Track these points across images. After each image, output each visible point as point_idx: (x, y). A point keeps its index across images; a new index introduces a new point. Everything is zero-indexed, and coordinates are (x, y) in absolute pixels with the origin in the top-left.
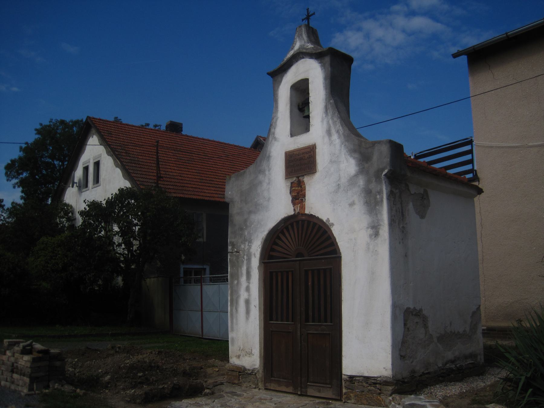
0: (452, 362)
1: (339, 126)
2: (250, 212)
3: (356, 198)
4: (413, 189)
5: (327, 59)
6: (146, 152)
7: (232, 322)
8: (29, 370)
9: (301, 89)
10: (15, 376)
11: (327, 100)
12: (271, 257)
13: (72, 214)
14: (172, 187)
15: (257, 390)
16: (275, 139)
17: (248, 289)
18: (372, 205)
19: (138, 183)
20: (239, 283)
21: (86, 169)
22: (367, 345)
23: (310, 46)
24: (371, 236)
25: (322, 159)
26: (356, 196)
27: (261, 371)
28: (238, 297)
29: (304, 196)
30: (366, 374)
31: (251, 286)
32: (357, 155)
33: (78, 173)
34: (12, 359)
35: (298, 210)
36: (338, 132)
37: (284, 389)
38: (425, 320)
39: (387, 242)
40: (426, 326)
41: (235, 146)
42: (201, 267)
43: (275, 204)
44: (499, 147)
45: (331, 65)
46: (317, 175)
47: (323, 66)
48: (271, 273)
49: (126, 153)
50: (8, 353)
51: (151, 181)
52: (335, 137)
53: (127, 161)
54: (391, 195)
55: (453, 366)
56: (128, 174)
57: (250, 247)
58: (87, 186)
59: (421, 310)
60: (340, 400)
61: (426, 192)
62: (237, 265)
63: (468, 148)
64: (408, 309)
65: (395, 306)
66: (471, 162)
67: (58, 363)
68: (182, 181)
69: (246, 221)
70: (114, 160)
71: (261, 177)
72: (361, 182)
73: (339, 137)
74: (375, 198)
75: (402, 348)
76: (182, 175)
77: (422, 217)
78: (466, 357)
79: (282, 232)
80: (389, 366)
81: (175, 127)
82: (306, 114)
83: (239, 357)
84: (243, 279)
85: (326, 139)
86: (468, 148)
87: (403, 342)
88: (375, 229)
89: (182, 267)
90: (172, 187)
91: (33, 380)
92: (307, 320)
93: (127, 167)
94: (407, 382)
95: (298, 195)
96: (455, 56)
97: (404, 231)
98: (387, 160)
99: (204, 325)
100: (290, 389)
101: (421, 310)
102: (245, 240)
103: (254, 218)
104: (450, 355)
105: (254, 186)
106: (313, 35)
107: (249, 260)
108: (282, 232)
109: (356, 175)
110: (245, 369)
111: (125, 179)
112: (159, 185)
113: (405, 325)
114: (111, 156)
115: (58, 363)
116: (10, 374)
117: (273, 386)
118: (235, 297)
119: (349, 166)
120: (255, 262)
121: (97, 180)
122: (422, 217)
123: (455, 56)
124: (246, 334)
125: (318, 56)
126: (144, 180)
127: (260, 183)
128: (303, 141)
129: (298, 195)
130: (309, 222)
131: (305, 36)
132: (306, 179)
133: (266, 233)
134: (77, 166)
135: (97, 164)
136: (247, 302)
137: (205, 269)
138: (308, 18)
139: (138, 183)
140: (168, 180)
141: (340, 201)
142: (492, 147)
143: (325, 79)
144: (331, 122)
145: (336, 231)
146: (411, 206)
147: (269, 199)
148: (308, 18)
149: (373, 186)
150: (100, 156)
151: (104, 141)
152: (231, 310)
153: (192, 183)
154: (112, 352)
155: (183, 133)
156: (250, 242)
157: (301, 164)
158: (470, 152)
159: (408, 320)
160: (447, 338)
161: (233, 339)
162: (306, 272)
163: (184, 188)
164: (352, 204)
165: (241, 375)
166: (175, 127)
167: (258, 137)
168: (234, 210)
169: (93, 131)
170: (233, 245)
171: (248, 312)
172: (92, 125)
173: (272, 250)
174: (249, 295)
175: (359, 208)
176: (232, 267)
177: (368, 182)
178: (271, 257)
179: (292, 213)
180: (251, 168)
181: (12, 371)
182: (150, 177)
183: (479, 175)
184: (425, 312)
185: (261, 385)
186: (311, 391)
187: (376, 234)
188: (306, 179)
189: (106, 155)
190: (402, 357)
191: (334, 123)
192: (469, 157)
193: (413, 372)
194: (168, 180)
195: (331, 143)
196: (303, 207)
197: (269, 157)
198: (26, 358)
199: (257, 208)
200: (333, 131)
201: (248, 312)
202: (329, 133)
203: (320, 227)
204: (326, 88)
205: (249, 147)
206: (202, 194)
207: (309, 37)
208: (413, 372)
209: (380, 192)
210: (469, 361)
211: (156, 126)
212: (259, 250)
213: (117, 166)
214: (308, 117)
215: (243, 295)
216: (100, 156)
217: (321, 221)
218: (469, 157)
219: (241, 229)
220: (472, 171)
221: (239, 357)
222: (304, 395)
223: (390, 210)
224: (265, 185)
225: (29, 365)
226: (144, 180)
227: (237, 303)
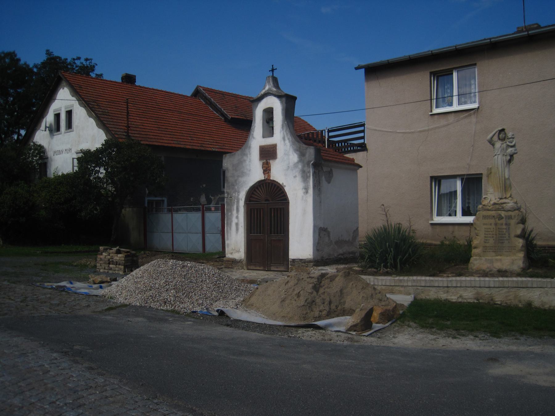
0: (342, 255)
1: (289, 135)
2: (238, 176)
3: (297, 174)
4: (325, 169)
5: (284, 99)
6: (174, 139)
7: (228, 235)
8: (124, 262)
9: (269, 113)
10: (111, 266)
11: (283, 122)
12: (250, 201)
13: (44, 153)
14: (138, 136)
15: (243, 270)
16: (254, 138)
17: (237, 217)
18: (305, 178)
19: (113, 133)
20: (232, 214)
21: (57, 116)
22: (301, 243)
23: (274, 89)
24: (304, 193)
25: (280, 152)
26: (297, 172)
27: (245, 260)
28: (231, 222)
29: (270, 170)
30: (301, 258)
31: (239, 216)
32: (298, 152)
33: (49, 118)
34: (109, 257)
35: (266, 177)
36: (289, 139)
37: (258, 268)
38: (329, 233)
39: (312, 196)
40: (329, 236)
41: (179, 95)
42: (161, 199)
43: (254, 173)
44: (380, 131)
45: (286, 103)
46: (277, 160)
47: (282, 102)
48: (251, 209)
49: (97, 105)
50: (104, 254)
51: (122, 130)
52: (287, 141)
53: (100, 113)
54: (314, 173)
55: (342, 257)
56: (102, 123)
57: (238, 195)
58: (58, 129)
59: (327, 228)
60: (288, 271)
61: (331, 170)
62: (231, 204)
63: (362, 128)
64: (321, 227)
65: (315, 226)
66: (363, 138)
67: (135, 259)
68: (144, 130)
69: (236, 181)
70: (87, 111)
71: (245, 158)
72: (300, 166)
73: (289, 142)
74: (307, 175)
75: (318, 245)
76: (144, 124)
77: (329, 182)
78: (349, 253)
79: (257, 188)
80: (312, 253)
81: (129, 79)
82: (271, 126)
83: (232, 253)
84: (235, 212)
85: (283, 142)
86: (362, 128)
87: (318, 243)
88: (306, 190)
89: (147, 199)
90: (138, 136)
91: (126, 267)
92: (271, 233)
93: (102, 119)
94: (318, 261)
95: (267, 169)
96: (357, 69)
97: (320, 190)
98: (313, 157)
99: (174, 243)
100: (261, 268)
101: (327, 228)
102: (235, 191)
103: (242, 179)
104: (341, 251)
105: (241, 162)
106: (275, 81)
107: (238, 202)
108: (257, 188)
109: (298, 163)
110: (236, 260)
111: (99, 128)
112: (130, 134)
113: (319, 235)
114: (85, 107)
115: (135, 259)
116: (107, 265)
117: (252, 267)
118: (229, 222)
119: (294, 157)
120: (242, 203)
121: (69, 125)
122: (329, 182)
123: (357, 69)
124: (236, 242)
125: (279, 97)
126: (117, 130)
127: (245, 161)
128: (269, 141)
129: (267, 169)
130: (272, 184)
131: (271, 83)
132: (271, 162)
133: (248, 188)
134: (48, 113)
135: (69, 113)
136: (237, 224)
137: (163, 201)
138: (273, 70)
139: (113, 133)
140: (134, 129)
141: (289, 172)
142: (376, 130)
143: (283, 110)
144: (285, 133)
145: (286, 189)
146: (323, 178)
147: (250, 170)
148: (273, 70)
149: (306, 169)
150: (73, 106)
151: (76, 92)
152: (227, 229)
153: (153, 131)
154: (145, 256)
155: (137, 83)
156: (239, 192)
157: (268, 154)
158: (363, 131)
159: (321, 233)
160: (340, 243)
161: (228, 244)
162: (271, 209)
163: (148, 136)
164: (295, 177)
165: (233, 263)
166: (129, 79)
167: (198, 87)
168: (228, 174)
169: (64, 83)
170: (228, 194)
171: (237, 229)
172: (63, 77)
173: (251, 197)
174: (238, 221)
175: (299, 179)
176: (228, 205)
177: (304, 166)
178: (250, 201)
179: (263, 179)
180: (239, 152)
181: (109, 264)
182: (122, 127)
183: (367, 147)
184: (329, 230)
185: (245, 267)
186: (273, 268)
187: (307, 192)
188: (271, 162)
189: (78, 106)
190: (318, 250)
191: (287, 134)
192: (361, 135)
193: (323, 257)
194: (134, 129)
195: (285, 144)
196: (269, 176)
197: (250, 147)
198: (120, 255)
199: (243, 174)
200: (286, 138)
201: (237, 229)
202: (284, 139)
203: (278, 187)
204: (283, 115)
205: (189, 94)
206: (161, 141)
207: (273, 84)
208: (323, 257)
209: (309, 172)
210: (351, 255)
211: (87, 60)
212: (244, 197)
213: (90, 116)
214: (273, 127)
215: (234, 221)
216: (73, 106)
217: (279, 184)
218: (361, 135)
219: (233, 185)
220: (364, 143)
221: (232, 253)
222: (269, 270)
223: (314, 181)
224: (247, 162)
225: (123, 259)
226: (117, 130)
227: (231, 224)
